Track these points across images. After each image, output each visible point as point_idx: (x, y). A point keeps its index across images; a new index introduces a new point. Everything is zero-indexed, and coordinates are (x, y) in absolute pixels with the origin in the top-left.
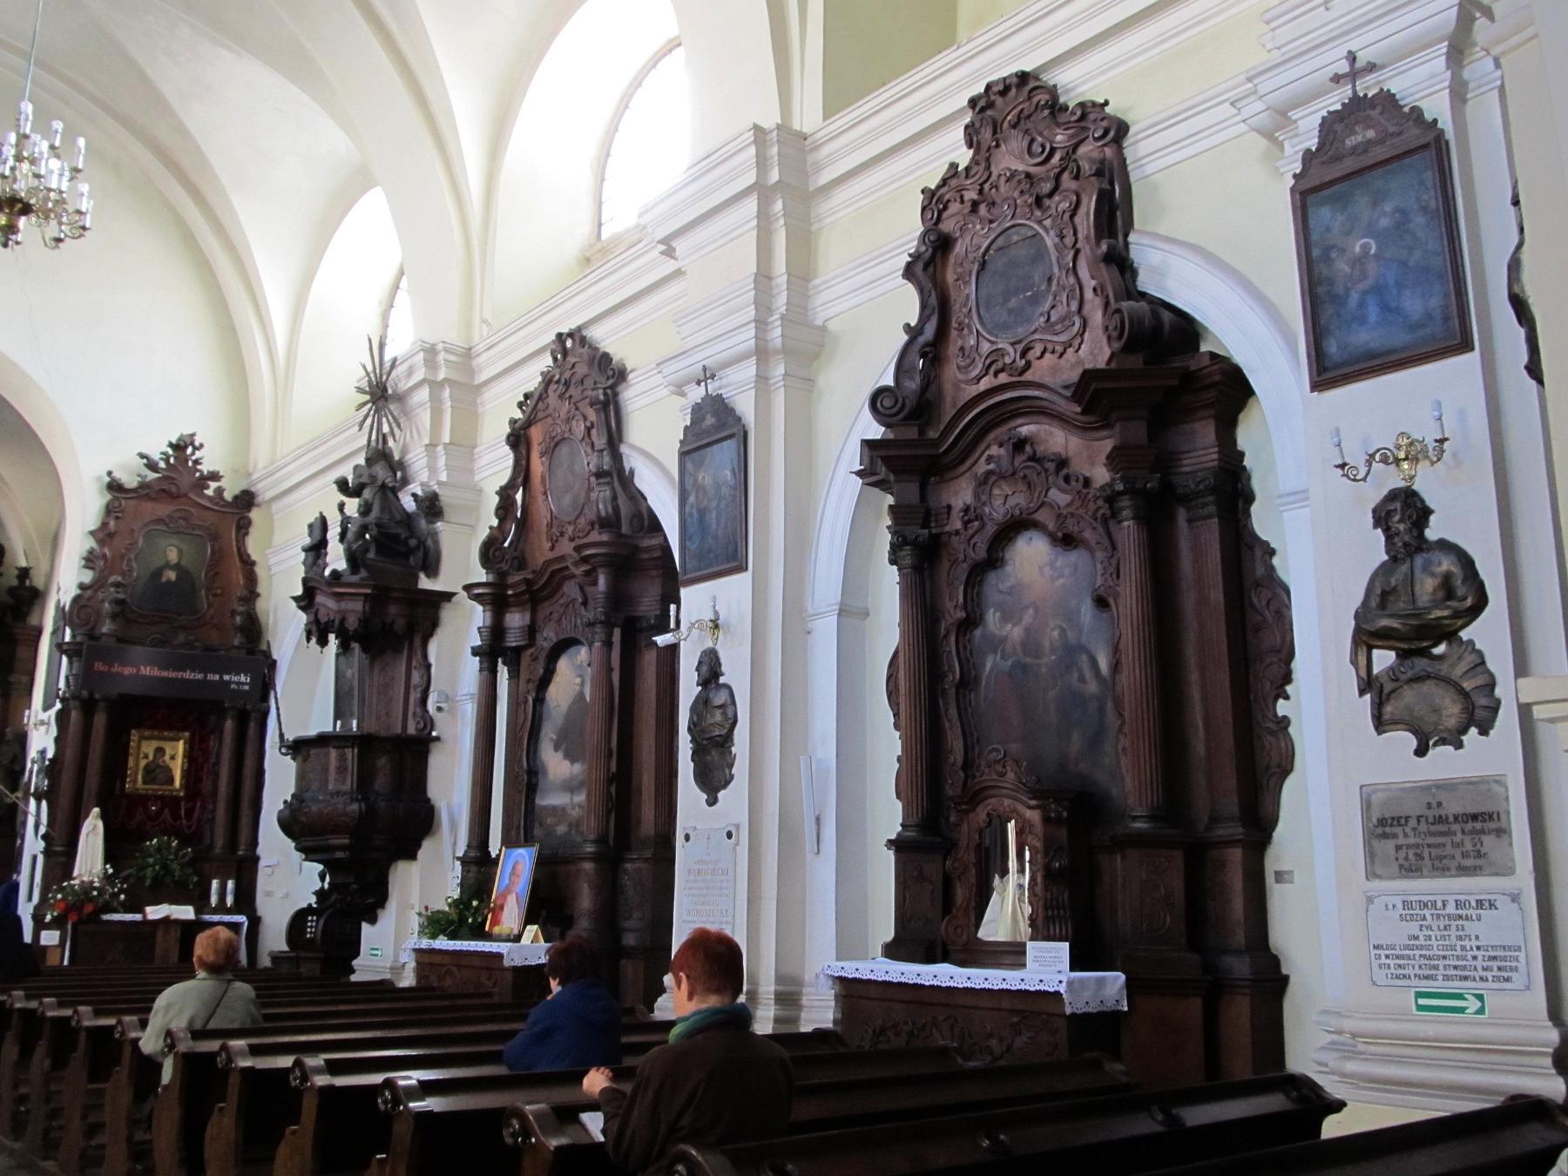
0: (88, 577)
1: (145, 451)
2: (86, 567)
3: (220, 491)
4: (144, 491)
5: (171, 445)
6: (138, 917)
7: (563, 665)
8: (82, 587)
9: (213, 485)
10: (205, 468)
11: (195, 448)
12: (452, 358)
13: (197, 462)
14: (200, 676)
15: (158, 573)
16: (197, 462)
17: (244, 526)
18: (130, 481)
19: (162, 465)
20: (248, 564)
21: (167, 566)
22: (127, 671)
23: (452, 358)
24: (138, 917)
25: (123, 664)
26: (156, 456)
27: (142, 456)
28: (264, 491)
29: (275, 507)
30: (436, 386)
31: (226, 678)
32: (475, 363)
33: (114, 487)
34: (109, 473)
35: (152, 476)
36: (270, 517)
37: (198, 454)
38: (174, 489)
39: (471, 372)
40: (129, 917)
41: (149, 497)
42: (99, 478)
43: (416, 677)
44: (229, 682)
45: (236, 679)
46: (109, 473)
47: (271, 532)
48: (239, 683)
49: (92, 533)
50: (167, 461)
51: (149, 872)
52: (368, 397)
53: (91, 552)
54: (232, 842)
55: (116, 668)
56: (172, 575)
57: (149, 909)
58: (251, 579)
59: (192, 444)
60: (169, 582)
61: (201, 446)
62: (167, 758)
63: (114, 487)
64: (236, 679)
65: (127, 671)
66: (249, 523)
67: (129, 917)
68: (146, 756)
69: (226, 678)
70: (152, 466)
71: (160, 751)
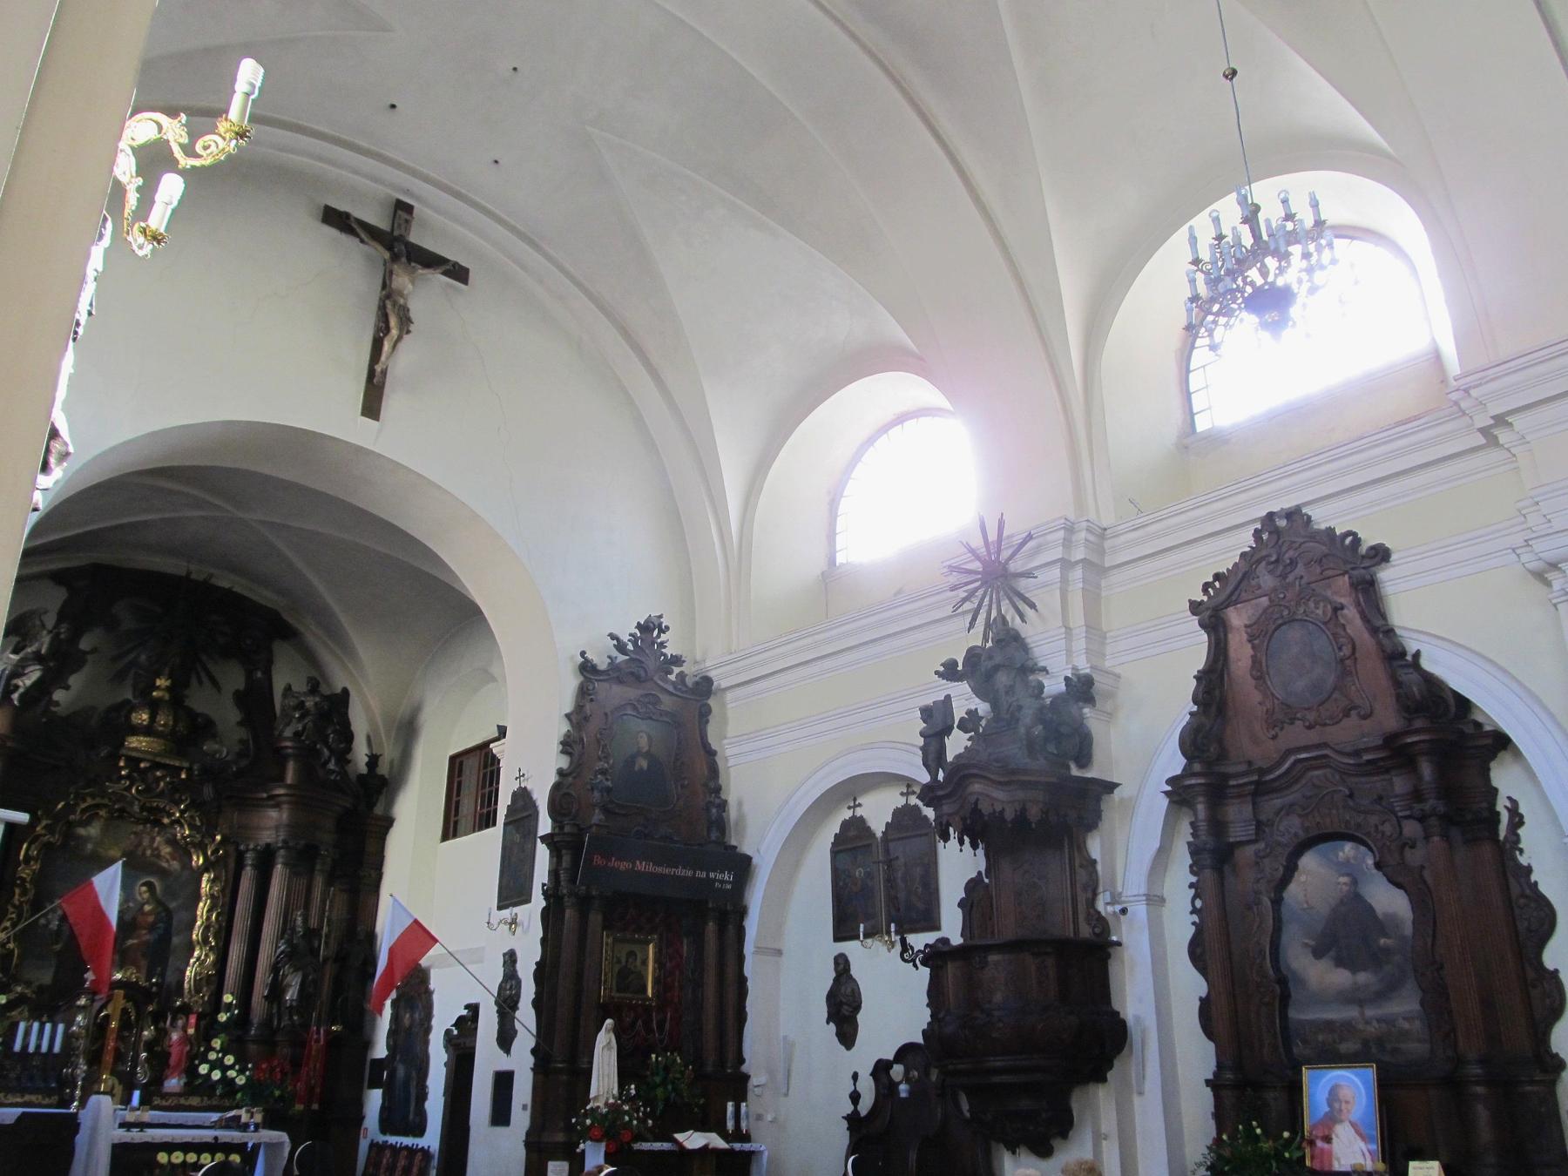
0: (564, 762)
1: (616, 632)
2: (562, 752)
3: (682, 676)
4: (615, 673)
5: (639, 626)
6: (666, 1146)
7: (1309, 861)
8: (560, 772)
9: (676, 670)
10: (669, 651)
11: (662, 631)
12: (1092, 538)
13: (662, 645)
14: (689, 873)
15: (631, 761)
16: (662, 645)
17: (705, 714)
18: (602, 663)
19: (630, 647)
20: (711, 753)
21: (639, 753)
22: (624, 866)
23: (1092, 538)
24: (666, 1146)
25: (620, 859)
26: (625, 638)
27: (613, 637)
28: (721, 679)
29: (729, 696)
30: (1066, 564)
31: (712, 875)
32: (1107, 544)
33: (587, 668)
34: (583, 654)
35: (621, 658)
36: (723, 705)
37: (663, 637)
38: (642, 673)
39: (1102, 552)
40: (657, 1146)
41: (620, 681)
42: (572, 658)
43: (1082, 876)
44: (715, 880)
45: (719, 876)
46: (583, 654)
47: (724, 721)
48: (722, 882)
49: (568, 716)
50: (635, 643)
51: (659, 1092)
52: (1014, 566)
53: (568, 735)
54: (722, 1063)
55: (614, 863)
56: (643, 763)
57: (679, 1137)
58: (714, 771)
59: (660, 625)
60: (641, 769)
61: (667, 628)
62: (638, 963)
63: (587, 668)
64: (719, 876)
65: (624, 866)
66: (709, 711)
67: (657, 1146)
68: (619, 961)
69: (712, 875)
70: (621, 647)
71: (632, 954)
